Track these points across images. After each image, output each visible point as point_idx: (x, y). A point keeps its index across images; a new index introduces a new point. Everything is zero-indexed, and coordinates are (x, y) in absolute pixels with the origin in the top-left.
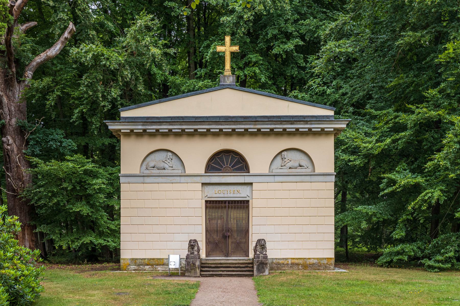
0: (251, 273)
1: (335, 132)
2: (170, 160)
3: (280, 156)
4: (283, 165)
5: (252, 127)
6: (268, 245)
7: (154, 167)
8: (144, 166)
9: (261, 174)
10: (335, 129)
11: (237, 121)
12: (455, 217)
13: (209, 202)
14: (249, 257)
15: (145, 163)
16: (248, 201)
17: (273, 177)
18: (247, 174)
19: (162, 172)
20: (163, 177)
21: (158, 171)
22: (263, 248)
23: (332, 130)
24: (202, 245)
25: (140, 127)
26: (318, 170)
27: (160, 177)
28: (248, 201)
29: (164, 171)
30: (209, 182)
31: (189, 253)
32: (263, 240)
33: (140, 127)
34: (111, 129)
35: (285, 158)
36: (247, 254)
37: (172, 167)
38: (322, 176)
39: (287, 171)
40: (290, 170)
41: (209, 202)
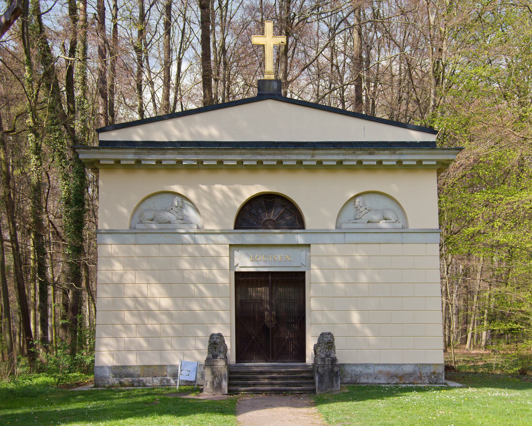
0: (312, 387)
1: (438, 167)
2: (179, 208)
3: (352, 203)
4: (357, 217)
5: (309, 158)
6: (338, 343)
7: (152, 220)
8: (136, 219)
9: (316, 230)
10: (439, 162)
11: (445, 328)
12: (260, 211)
13: (241, 274)
14: (305, 362)
15: (138, 213)
16: (304, 273)
17: (400, 234)
18: (302, 231)
19: (166, 227)
20: (167, 235)
21: (160, 226)
22: (329, 346)
23: (435, 163)
24: (230, 343)
25: (131, 157)
26: (412, 226)
27: (163, 235)
28: (304, 273)
29: (168, 225)
30: (241, 243)
31: (211, 356)
32: (329, 334)
33: (131, 157)
34: (83, 159)
35: (361, 207)
36: (301, 356)
37: (182, 220)
38: (421, 234)
39: (365, 227)
40: (369, 225)
41: (241, 274)
